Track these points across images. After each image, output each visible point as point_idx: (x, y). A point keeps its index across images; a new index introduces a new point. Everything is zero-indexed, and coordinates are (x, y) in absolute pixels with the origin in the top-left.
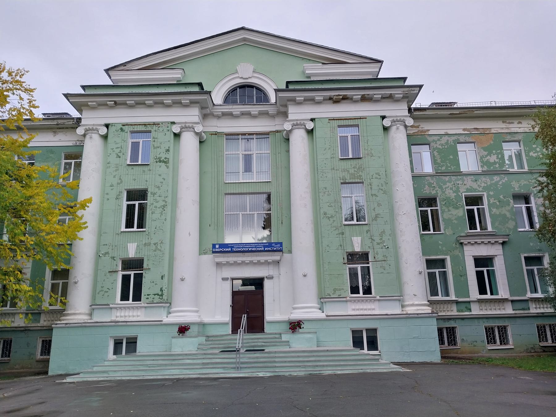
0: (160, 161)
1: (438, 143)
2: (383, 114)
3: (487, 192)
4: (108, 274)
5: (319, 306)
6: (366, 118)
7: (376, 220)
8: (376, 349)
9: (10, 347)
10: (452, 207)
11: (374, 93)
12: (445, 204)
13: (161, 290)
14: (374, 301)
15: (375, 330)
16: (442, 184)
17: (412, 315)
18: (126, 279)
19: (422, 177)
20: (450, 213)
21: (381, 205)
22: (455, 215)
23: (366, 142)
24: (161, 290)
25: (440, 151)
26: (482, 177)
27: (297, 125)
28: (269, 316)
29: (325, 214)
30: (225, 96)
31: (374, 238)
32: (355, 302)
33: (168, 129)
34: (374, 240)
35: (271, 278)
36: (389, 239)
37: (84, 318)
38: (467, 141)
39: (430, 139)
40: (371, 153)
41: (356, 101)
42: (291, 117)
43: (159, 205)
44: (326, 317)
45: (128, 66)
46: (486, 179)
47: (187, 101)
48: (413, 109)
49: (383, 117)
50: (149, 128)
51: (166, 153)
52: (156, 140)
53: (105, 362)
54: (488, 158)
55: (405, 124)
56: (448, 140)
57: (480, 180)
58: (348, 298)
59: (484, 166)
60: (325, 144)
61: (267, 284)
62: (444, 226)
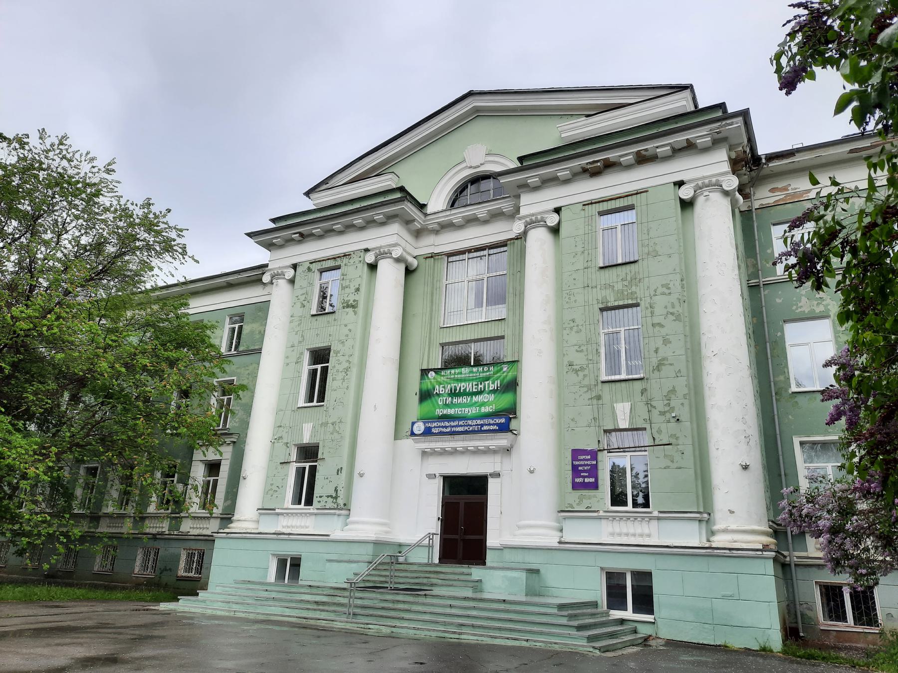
0: (348, 306)
2: (678, 178)
4: (280, 466)
5: (556, 524)
6: (646, 191)
8: (650, 611)
9: (202, 561)
11: (655, 145)
13: (336, 490)
17: (718, 551)
18: (300, 472)
21: (670, 342)
23: (646, 232)
24: (336, 490)
27: (533, 223)
28: (492, 540)
29: (570, 365)
31: (654, 403)
32: (622, 520)
33: (360, 259)
34: (654, 407)
35: (497, 475)
36: (682, 404)
37: (249, 526)
40: (655, 250)
41: (629, 167)
42: (523, 211)
44: (557, 545)
45: (332, 183)
48: (763, 157)
49: (680, 184)
52: (345, 277)
53: (217, 588)
55: (723, 189)
58: (601, 513)
61: (492, 483)
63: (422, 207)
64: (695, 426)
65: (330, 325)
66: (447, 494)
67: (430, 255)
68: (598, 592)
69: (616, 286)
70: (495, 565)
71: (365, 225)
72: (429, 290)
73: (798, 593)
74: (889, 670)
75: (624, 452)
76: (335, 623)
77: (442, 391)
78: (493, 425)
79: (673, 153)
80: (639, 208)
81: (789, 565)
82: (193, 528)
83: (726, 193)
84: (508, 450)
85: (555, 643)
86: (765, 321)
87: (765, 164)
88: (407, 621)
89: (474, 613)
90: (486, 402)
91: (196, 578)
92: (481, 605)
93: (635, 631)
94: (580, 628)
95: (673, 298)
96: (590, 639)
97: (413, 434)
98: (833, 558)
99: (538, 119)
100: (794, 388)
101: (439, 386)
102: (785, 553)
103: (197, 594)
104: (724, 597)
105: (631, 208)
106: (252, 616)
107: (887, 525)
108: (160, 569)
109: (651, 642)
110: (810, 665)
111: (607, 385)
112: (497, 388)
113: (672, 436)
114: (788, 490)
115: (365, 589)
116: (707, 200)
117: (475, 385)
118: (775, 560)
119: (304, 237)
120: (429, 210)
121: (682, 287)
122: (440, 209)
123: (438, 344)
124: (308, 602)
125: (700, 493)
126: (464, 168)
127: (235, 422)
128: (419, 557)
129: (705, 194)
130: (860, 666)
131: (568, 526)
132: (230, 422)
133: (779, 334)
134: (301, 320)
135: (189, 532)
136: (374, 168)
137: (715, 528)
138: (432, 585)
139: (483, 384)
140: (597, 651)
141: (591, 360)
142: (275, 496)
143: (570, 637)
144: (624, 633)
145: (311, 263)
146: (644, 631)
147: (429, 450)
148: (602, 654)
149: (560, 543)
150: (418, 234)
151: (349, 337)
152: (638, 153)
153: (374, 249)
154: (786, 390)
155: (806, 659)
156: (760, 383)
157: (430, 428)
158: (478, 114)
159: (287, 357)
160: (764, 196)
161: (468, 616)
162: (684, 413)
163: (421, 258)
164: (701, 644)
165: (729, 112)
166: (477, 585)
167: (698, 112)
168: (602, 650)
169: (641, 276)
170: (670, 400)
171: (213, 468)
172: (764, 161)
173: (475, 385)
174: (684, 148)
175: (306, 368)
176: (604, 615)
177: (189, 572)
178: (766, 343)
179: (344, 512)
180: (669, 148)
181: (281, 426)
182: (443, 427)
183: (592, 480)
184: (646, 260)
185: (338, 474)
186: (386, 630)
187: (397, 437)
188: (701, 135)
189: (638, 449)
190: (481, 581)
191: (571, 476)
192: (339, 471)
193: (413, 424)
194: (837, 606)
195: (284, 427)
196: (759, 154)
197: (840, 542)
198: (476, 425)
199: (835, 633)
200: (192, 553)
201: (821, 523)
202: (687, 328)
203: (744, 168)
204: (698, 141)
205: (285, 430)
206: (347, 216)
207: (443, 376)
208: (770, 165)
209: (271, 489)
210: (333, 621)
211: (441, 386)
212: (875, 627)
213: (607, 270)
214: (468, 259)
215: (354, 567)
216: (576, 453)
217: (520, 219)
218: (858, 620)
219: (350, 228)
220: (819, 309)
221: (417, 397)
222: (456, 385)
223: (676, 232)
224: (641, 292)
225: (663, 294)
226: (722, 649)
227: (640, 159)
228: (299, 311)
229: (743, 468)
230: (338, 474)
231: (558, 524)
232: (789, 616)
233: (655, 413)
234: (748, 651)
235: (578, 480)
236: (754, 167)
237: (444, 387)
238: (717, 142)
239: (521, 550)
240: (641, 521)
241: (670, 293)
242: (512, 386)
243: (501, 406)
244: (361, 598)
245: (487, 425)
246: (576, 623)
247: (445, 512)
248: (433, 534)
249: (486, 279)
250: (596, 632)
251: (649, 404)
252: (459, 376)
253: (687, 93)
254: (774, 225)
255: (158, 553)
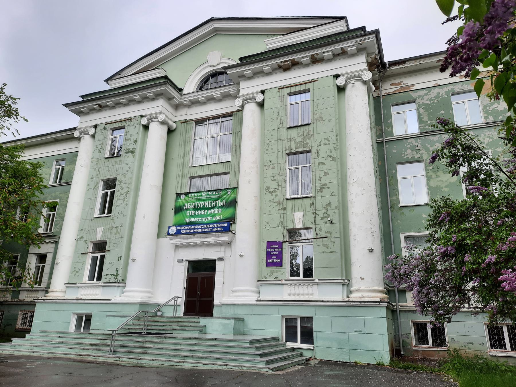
0: (129, 152)
1: (426, 97)
2: (336, 72)
3: (493, 149)
4: (81, 256)
7: (321, 192)
10: (442, 171)
11: (323, 51)
12: (433, 169)
13: (117, 271)
14: (313, 284)
15: (310, 319)
16: (429, 146)
17: (353, 303)
18: (94, 259)
19: (403, 140)
20: (439, 179)
22: (446, 181)
24: (117, 271)
25: (427, 107)
26: (486, 131)
27: (247, 100)
28: (217, 301)
30: (198, 86)
32: (300, 286)
33: (138, 122)
34: (318, 215)
35: (221, 259)
36: (335, 212)
38: (465, 90)
39: (414, 95)
40: (321, 117)
41: (307, 65)
42: (242, 92)
43: (123, 192)
44: (255, 302)
45: (123, 74)
46: (491, 133)
47: (151, 94)
48: (387, 63)
49: (337, 76)
50: (124, 124)
51: (134, 144)
54: (495, 107)
55: (363, 80)
56: (439, 93)
57: (482, 135)
58: (284, 281)
59: (489, 116)
60: (273, 114)
61: (218, 264)
62: (430, 195)
63: (180, 90)
64: (342, 226)
65: (116, 164)
66: (191, 272)
67: (184, 121)
68: (280, 332)
69: (297, 139)
70: (218, 316)
71: (141, 100)
72: (183, 143)
73: (401, 329)
74: (452, 374)
75: (299, 243)
76: (100, 358)
77: (189, 207)
78: (220, 227)
79: (333, 57)
80: (312, 91)
81: (396, 311)
82: (28, 297)
83: (365, 83)
84: (229, 244)
85: (245, 367)
86: (386, 163)
87: (388, 68)
88: (149, 355)
89: (196, 348)
90: (216, 214)
91: (28, 329)
92: (201, 342)
93: (301, 355)
94: (262, 355)
95: (331, 147)
96: (268, 363)
97: (169, 234)
98: (421, 304)
99: (254, 37)
100: (402, 204)
101: (187, 204)
102: (393, 304)
103: (11, 341)
104: (356, 332)
105: (307, 91)
106: (45, 355)
107: (458, 278)
108: (4, 324)
109: (311, 362)
110: (406, 373)
111: (289, 201)
112: (224, 205)
113: (328, 232)
114: (391, 257)
115: (125, 334)
116: (353, 86)
117: (210, 203)
118: (387, 308)
119: (101, 108)
120: (184, 92)
121: (337, 140)
122: (191, 91)
123: (188, 178)
124: (86, 344)
125: (344, 267)
126: (207, 66)
127: (57, 229)
128: (169, 312)
129: (352, 82)
130: (435, 371)
131: (263, 289)
132: (54, 228)
133: (394, 171)
134: (98, 161)
135: (25, 300)
136: (150, 66)
137: (352, 289)
138: (173, 330)
139: (215, 202)
140: (271, 371)
141: (280, 186)
142: (77, 275)
143: (254, 362)
144: (292, 357)
145: (106, 124)
146: (307, 355)
147: (179, 244)
148: (274, 373)
149: (257, 301)
150: (177, 107)
151: (129, 172)
152: (312, 56)
153: (147, 115)
154: (397, 206)
155: (404, 369)
156: (382, 201)
157: (180, 230)
158: (216, 32)
159: (88, 185)
160: (387, 88)
161: (190, 351)
162: (335, 218)
163: (178, 123)
164: (341, 362)
165: (367, 31)
166: (203, 330)
167: (349, 31)
168: (274, 370)
169: (312, 133)
170: (327, 210)
171: (42, 258)
172: (387, 66)
173: (210, 203)
174: (340, 54)
175: (100, 192)
176: (283, 346)
177: (23, 326)
178: (386, 176)
179: (121, 285)
180: (331, 53)
181: (82, 230)
182: (188, 229)
183: (279, 261)
184: (315, 123)
185: (118, 260)
186: (134, 362)
187: (159, 236)
188: (350, 45)
189: (307, 241)
190: (205, 326)
191: (266, 259)
192: (119, 258)
193: (169, 227)
194: (423, 335)
195: (84, 231)
196: (385, 61)
197: (426, 292)
198: (209, 228)
199: (421, 352)
200: (26, 314)
201: (413, 279)
202: (339, 165)
203: (376, 69)
204: (348, 49)
205: (85, 232)
206: (129, 94)
207: (190, 197)
208: (391, 69)
209: (75, 271)
210: (99, 357)
211: (189, 204)
212: (444, 347)
213: (292, 129)
214: (208, 124)
215: (124, 320)
216: (270, 244)
217: (240, 97)
218: (435, 343)
219: (131, 102)
220: (417, 157)
221: (173, 211)
222: (198, 203)
223: (334, 106)
224: (312, 143)
225: (325, 144)
226: (354, 365)
227: (314, 61)
228: (97, 155)
229: (370, 252)
230: (118, 260)
231: (258, 289)
232: (395, 342)
233: (318, 218)
234: (369, 366)
235: (270, 261)
236: (382, 69)
237: (191, 205)
238: (360, 51)
239: (233, 306)
240: (307, 286)
241: (329, 144)
242: (233, 203)
243: (226, 216)
244: (122, 341)
245: (216, 227)
246: (259, 352)
247: (189, 284)
248: (178, 297)
249: (219, 137)
250: (273, 358)
251: (314, 213)
252: (200, 197)
253: (343, 22)
254: (393, 106)
255: (3, 313)
